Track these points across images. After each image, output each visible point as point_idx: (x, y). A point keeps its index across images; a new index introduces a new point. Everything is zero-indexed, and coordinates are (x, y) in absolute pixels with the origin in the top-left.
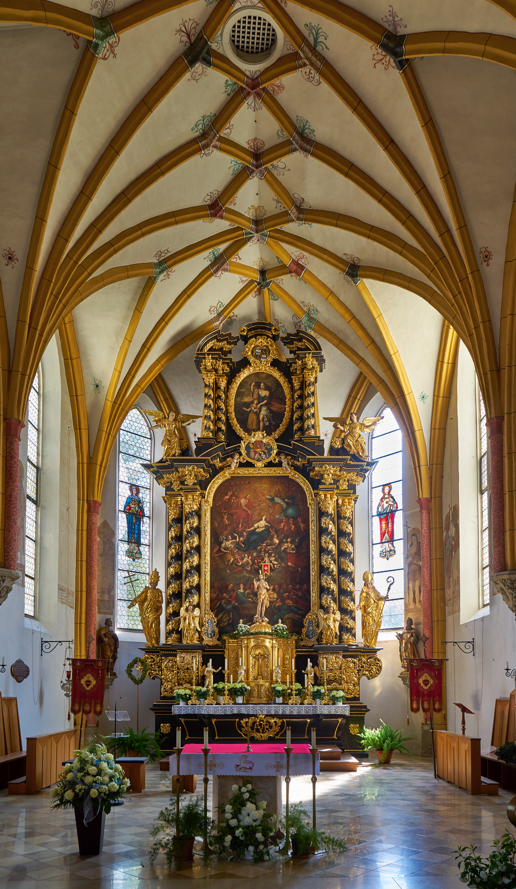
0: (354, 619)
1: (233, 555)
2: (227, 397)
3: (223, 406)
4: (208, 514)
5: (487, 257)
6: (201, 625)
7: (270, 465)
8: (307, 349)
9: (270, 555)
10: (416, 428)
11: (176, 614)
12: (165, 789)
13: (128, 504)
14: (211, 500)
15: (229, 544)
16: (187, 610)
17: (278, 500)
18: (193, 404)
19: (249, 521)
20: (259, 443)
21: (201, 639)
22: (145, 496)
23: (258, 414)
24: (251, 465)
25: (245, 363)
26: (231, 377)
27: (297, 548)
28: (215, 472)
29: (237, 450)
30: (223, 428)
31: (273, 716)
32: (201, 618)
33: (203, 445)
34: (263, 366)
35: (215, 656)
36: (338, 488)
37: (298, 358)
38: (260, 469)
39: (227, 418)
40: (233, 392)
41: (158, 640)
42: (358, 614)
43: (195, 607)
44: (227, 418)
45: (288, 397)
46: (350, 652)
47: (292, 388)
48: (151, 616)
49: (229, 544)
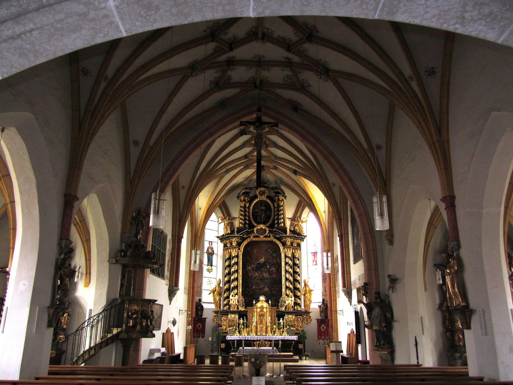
0: (300, 299)
1: (251, 272)
2: (249, 210)
3: (247, 214)
4: (241, 256)
5: (334, 185)
6: (238, 302)
7: (266, 237)
8: (280, 193)
9: (266, 273)
10: (322, 223)
11: (228, 297)
12: (335, 356)
13: (208, 249)
14: (242, 251)
15: (249, 268)
16: (233, 296)
17: (269, 250)
18: (236, 213)
19: (257, 259)
20: (261, 229)
21: (238, 308)
22: (214, 246)
23: (261, 216)
24: (259, 237)
25: (256, 197)
26: (250, 202)
27: (277, 270)
28: (244, 239)
29: (253, 231)
30: (247, 222)
31: (267, 340)
32: (238, 300)
33: (239, 230)
34: (264, 198)
35: (242, 315)
36: (293, 246)
37: (276, 196)
38: (262, 238)
39: (249, 218)
40: (251, 208)
41: (220, 308)
42: (302, 298)
43: (236, 295)
44: (249, 218)
45: (273, 210)
46: (298, 313)
47: (274, 206)
48: (217, 298)
49: (249, 268)
